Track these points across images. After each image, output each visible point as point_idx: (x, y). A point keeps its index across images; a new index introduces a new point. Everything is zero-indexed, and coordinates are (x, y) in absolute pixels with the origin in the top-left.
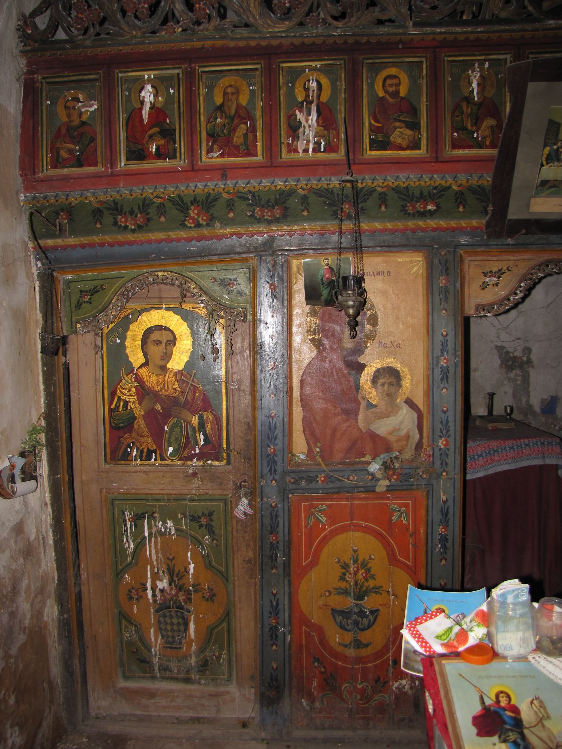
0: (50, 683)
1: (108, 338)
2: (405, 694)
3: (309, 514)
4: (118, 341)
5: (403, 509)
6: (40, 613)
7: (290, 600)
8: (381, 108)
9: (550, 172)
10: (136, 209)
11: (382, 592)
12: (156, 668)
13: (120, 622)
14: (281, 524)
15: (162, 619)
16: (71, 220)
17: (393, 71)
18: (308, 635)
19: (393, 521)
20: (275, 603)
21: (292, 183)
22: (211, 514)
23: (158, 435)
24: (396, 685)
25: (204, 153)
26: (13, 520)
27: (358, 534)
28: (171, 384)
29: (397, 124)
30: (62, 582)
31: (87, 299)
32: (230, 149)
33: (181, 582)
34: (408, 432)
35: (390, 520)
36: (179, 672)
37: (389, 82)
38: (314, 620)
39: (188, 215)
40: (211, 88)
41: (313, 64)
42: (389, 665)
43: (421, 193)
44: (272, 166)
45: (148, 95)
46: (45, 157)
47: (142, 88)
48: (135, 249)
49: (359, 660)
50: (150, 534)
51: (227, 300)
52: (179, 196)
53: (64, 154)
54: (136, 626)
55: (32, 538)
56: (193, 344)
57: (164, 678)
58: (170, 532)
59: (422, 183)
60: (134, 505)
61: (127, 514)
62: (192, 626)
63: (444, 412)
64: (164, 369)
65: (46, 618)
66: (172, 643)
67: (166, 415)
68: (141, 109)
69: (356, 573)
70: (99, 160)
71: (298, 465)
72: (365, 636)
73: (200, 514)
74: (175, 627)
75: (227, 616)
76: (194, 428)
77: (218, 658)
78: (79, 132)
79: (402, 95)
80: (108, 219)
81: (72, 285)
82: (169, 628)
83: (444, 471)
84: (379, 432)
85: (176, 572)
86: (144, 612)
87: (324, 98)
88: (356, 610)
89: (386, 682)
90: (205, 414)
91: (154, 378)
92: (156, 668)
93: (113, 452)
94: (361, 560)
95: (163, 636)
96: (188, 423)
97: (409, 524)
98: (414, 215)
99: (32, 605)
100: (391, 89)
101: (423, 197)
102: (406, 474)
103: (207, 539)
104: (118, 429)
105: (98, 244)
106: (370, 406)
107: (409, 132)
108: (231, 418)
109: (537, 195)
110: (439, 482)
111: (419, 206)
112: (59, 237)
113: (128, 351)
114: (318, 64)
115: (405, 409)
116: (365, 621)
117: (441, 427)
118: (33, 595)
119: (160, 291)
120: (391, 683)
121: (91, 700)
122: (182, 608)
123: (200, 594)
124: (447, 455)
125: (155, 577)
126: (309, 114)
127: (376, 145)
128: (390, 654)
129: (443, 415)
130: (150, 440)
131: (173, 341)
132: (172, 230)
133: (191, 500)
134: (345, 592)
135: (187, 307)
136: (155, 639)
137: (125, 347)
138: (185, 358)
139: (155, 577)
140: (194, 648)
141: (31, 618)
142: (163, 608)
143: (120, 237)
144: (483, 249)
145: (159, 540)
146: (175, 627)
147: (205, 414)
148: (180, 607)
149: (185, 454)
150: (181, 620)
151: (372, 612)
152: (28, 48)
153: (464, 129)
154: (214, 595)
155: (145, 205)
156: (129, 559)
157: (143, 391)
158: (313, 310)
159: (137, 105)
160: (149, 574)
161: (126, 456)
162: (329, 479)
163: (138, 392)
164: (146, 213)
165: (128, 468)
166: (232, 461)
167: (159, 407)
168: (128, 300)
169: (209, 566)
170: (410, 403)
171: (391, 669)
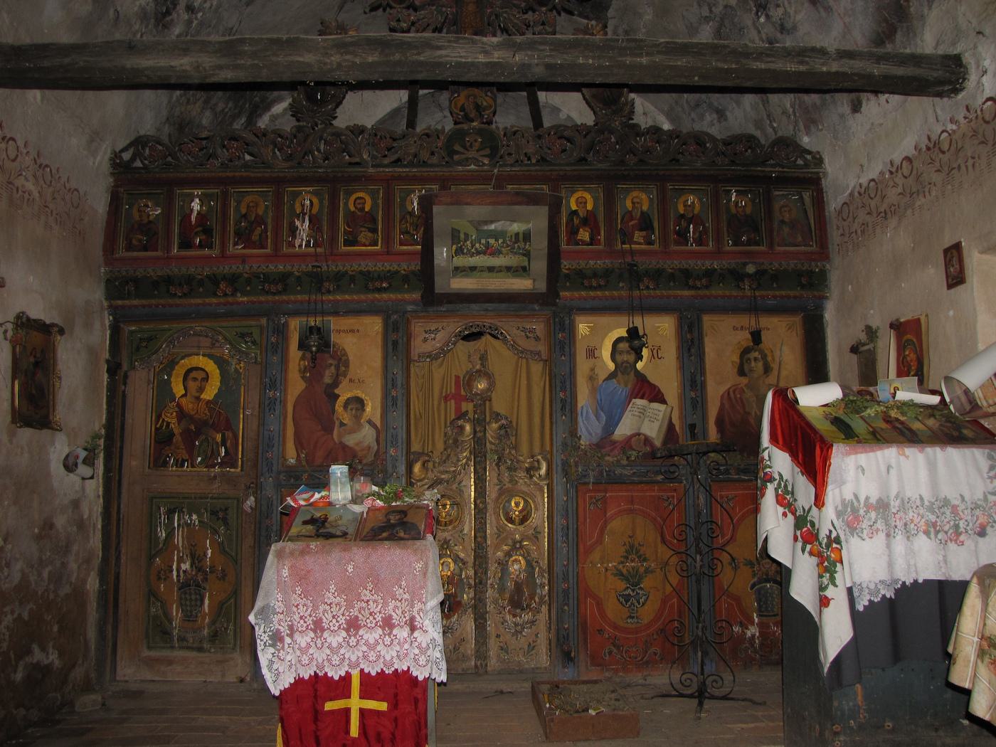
1: (158, 375)
8: (352, 218)
9: (460, 261)
12: (175, 639)
15: (183, 596)
17: (361, 194)
21: (289, 268)
22: (226, 509)
25: (231, 246)
29: (363, 229)
30: (105, 559)
31: (144, 344)
32: (249, 244)
36: (193, 643)
37: (358, 201)
39: (219, 288)
40: (239, 203)
41: (308, 189)
43: (379, 276)
44: (276, 255)
45: (196, 205)
46: (121, 242)
47: (193, 201)
52: (214, 275)
53: (134, 242)
54: (162, 602)
55: (85, 517)
57: (181, 648)
59: (377, 269)
62: (207, 602)
63: (394, 429)
64: (198, 398)
66: (189, 617)
67: (198, 433)
68: (191, 215)
70: (160, 247)
71: (289, 467)
74: (193, 603)
77: (226, 629)
78: (147, 228)
79: (366, 210)
82: (188, 603)
84: (347, 443)
87: (315, 211)
90: (226, 433)
92: (175, 639)
96: (214, 439)
98: (373, 290)
100: (359, 206)
101: (381, 278)
106: (342, 424)
107: (370, 235)
109: (454, 276)
111: (377, 284)
114: (311, 189)
115: (367, 426)
125: (180, 560)
126: (304, 222)
127: (347, 243)
130: (184, 452)
131: (206, 379)
133: (212, 498)
139: (180, 560)
140: (207, 620)
142: (184, 586)
143: (171, 301)
147: (226, 433)
148: (198, 585)
149: (210, 463)
152: (116, 171)
153: (408, 233)
154: (225, 575)
155: (189, 280)
156: (161, 546)
157: (182, 414)
158: (304, 355)
159: (188, 212)
160: (176, 558)
161: (165, 464)
164: (191, 285)
169: (223, 552)
170: (370, 422)
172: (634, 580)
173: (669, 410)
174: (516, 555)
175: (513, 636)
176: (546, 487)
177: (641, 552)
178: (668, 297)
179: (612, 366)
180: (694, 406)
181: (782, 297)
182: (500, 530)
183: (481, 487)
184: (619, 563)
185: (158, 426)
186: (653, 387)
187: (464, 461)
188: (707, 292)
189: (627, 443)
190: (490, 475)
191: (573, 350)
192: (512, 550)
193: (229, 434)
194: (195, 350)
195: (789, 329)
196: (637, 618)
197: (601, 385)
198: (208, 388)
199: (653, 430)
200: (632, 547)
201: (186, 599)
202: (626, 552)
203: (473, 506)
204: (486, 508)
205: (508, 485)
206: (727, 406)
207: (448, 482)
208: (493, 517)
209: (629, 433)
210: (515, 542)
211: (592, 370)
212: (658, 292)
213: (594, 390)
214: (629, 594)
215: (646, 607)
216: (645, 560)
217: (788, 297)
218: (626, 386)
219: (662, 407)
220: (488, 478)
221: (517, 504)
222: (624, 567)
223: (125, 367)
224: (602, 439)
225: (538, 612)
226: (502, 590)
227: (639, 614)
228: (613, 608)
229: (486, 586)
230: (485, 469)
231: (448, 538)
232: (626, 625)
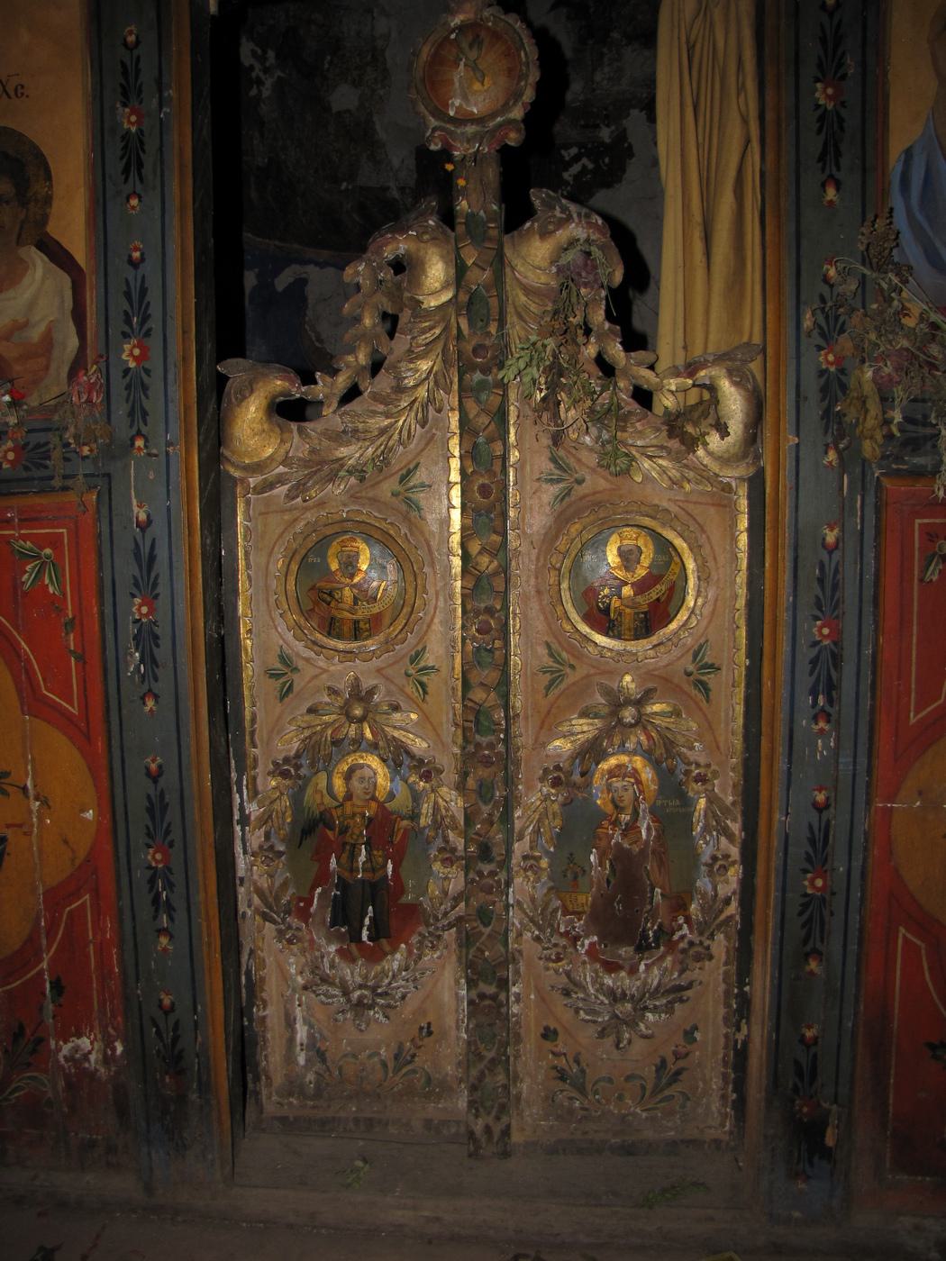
2: (92, 1075)
5: (48, 551)
11: (9, 789)
19: (26, 587)
24: (66, 1049)
34: (49, 331)
42: (44, 994)
63: (134, 264)
83: (139, 434)
89: (40, 1041)
97: (64, 595)
102: (38, 446)
110: (127, 467)
117: (126, 306)
120: (53, 1043)
124: (145, 388)
128: (45, 965)
129: (130, 273)
171: (51, 1007)
174: (622, 749)
175: (602, 1034)
176: (743, 491)
182: (563, 654)
183: (485, 491)
187: (422, 393)
190: (523, 449)
192: (607, 732)
203: (457, 562)
204: (504, 570)
205: (596, 483)
207: (359, 472)
208: (534, 605)
210: (617, 702)
220: (514, 456)
221: (629, 558)
225: (698, 958)
226: (568, 874)
229: (505, 863)
230: (501, 416)
231: (367, 683)
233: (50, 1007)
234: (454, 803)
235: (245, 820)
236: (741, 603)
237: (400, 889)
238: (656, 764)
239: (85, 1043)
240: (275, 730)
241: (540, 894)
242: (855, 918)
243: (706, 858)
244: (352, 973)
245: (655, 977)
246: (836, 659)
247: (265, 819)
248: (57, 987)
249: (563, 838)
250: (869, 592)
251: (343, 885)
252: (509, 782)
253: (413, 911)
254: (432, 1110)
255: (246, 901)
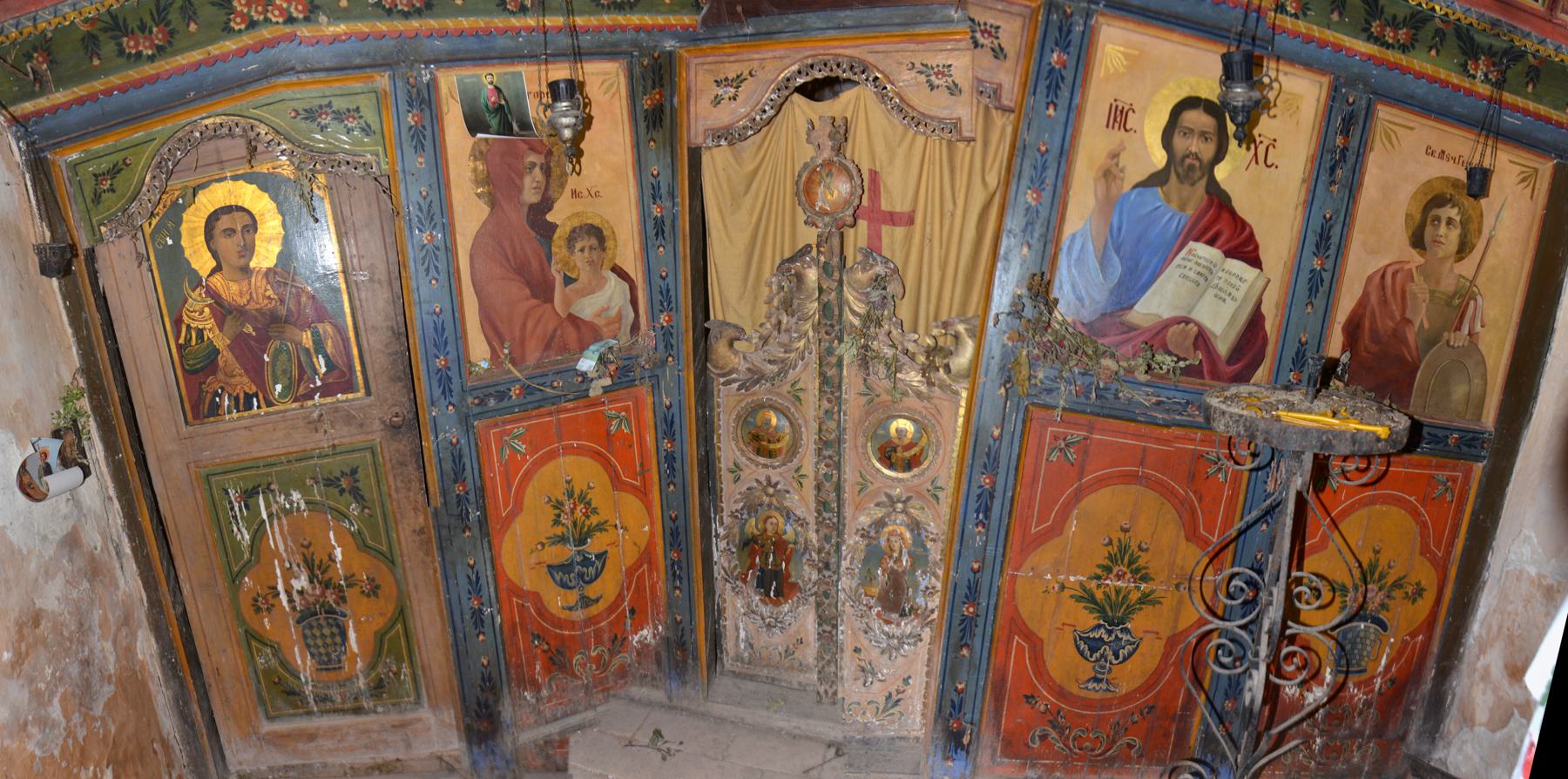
0: (165, 744)
1: (153, 241)
2: (648, 646)
3: (501, 445)
4: (170, 242)
6: (129, 651)
7: (493, 568)
10: (148, 20)
13: (249, 645)
14: (468, 466)
15: (307, 632)
16: (52, 63)
18: (522, 608)
20: (474, 578)
22: (354, 472)
23: (255, 370)
26: (62, 529)
27: (570, 459)
28: (261, 291)
30: (155, 604)
31: (106, 185)
33: (327, 577)
35: (608, 432)
36: (344, 701)
38: (527, 587)
39: (232, 10)
48: (160, 89)
49: (590, 621)
50: (270, 516)
51: (320, 141)
56: (284, 225)
57: (323, 712)
58: (298, 509)
60: (240, 478)
61: (231, 492)
62: (352, 635)
63: (663, 278)
64: (246, 271)
65: (140, 657)
66: (328, 662)
67: (263, 340)
69: (573, 511)
72: (592, 591)
73: (338, 474)
74: (329, 641)
75: (401, 614)
76: (307, 350)
77: (398, 674)
80: (108, 48)
81: (80, 169)
82: (320, 642)
85: (317, 562)
86: (280, 626)
88: (579, 559)
89: (625, 639)
90: (320, 327)
91: (234, 287)
93: (196, 408)
94: (577, 492)
95: (312, 655)
96: (298, 344)
99: (115, 643)
103: (354, 509)
104: (195, 372)
105: (102, 92)
108: (361, 325)
112: (42, 93)
113: (187, 254)
115: (613, 277)
116: (592, 570)
118: (113, 629)
119: (218, 152)
121: (227, 753)
122: (335, 612)
123: (357, 589)
125: (288, 574)
129: (661, 282)
130: (246, 379)
131: (252, 225)
132: (211, 41)
134: (562, 540)
135: (263, 168)
136: (303, 662)
137: (181, 250)
138: (276, 249)
139: (288, 574)
140: (359, 665)
141: (118, 660)
142: (306, 616)
143: (134, 74)
144: (711, 44)
145: (285, 521)
146: (329, 641)
147: (320, 327)
148: (330, 611)
149: (302, 390)
150: (335, 630)
151: (598, 556)
154: (378, 587)
157: (222, 310)
160: (278, 572)
161: (215, 409)
162: (527, 390)
163: (214, 313)
165: (221, 427)
166: (373, 390)
167: (249, 329)
168: (170, 174)
169: (364, 547)
172: (1113, 613)
173: (1261, 283)
175: (883, 652)
177: (1141, 562)
178: (1323, 44)
179: (1159, 158)
180: (1313, 290)
181: (1537, 116)
184: (1090, 578)
185: (181, 341)
186: (1240, 224)
188: (1403, 59)
189: (1156, 338)
191: (1076, 101)
193: (326, 329)
194: (216, 174)
195: (1523, 180)
196: (1108, 682)
197: (1127, 196)
198: (260, 247)
199: (1220, 321)
200: (1123, 549)
201: (315, 637)
202: (1110, 557)
206: (1374, 299)
209: (1167, 314)
210: (892, 501)
211: (1115, 156)
212: (1302, 26)
213: (1109, 203)
214: (1101, 639)
215: (1129, 665)
216: (1145, 579)
217: (1548, 120)
218: (1182, 208)
219: (1249, 273)
222: (1099, 586)
223: (84, 243)
224: (1103, 315)
226: (868, 579)
227: (1112, 675)
228: (1063, 661)
229: (837, 572)
232: (1083, 694)
233: (629, 622)
234: (813, 537)
235: (717, 536)
236: (955, 455)
237: (789, 576)
238: (912, 531)
239: (645, 632)
240: (731, 495)
241: (854, 585)
242: (989, 629)
243: (922, 587)
244: (765, 610)
245: (908, 630)
246: (992, 497)
247: (726, 536)
248: (632, 611)
249: (866, 561)
250: (1013, 463)
251: (762, 570)
252: (840, 534)
253: (794, 586)
254: (802, 678)
255: (718, 572)
